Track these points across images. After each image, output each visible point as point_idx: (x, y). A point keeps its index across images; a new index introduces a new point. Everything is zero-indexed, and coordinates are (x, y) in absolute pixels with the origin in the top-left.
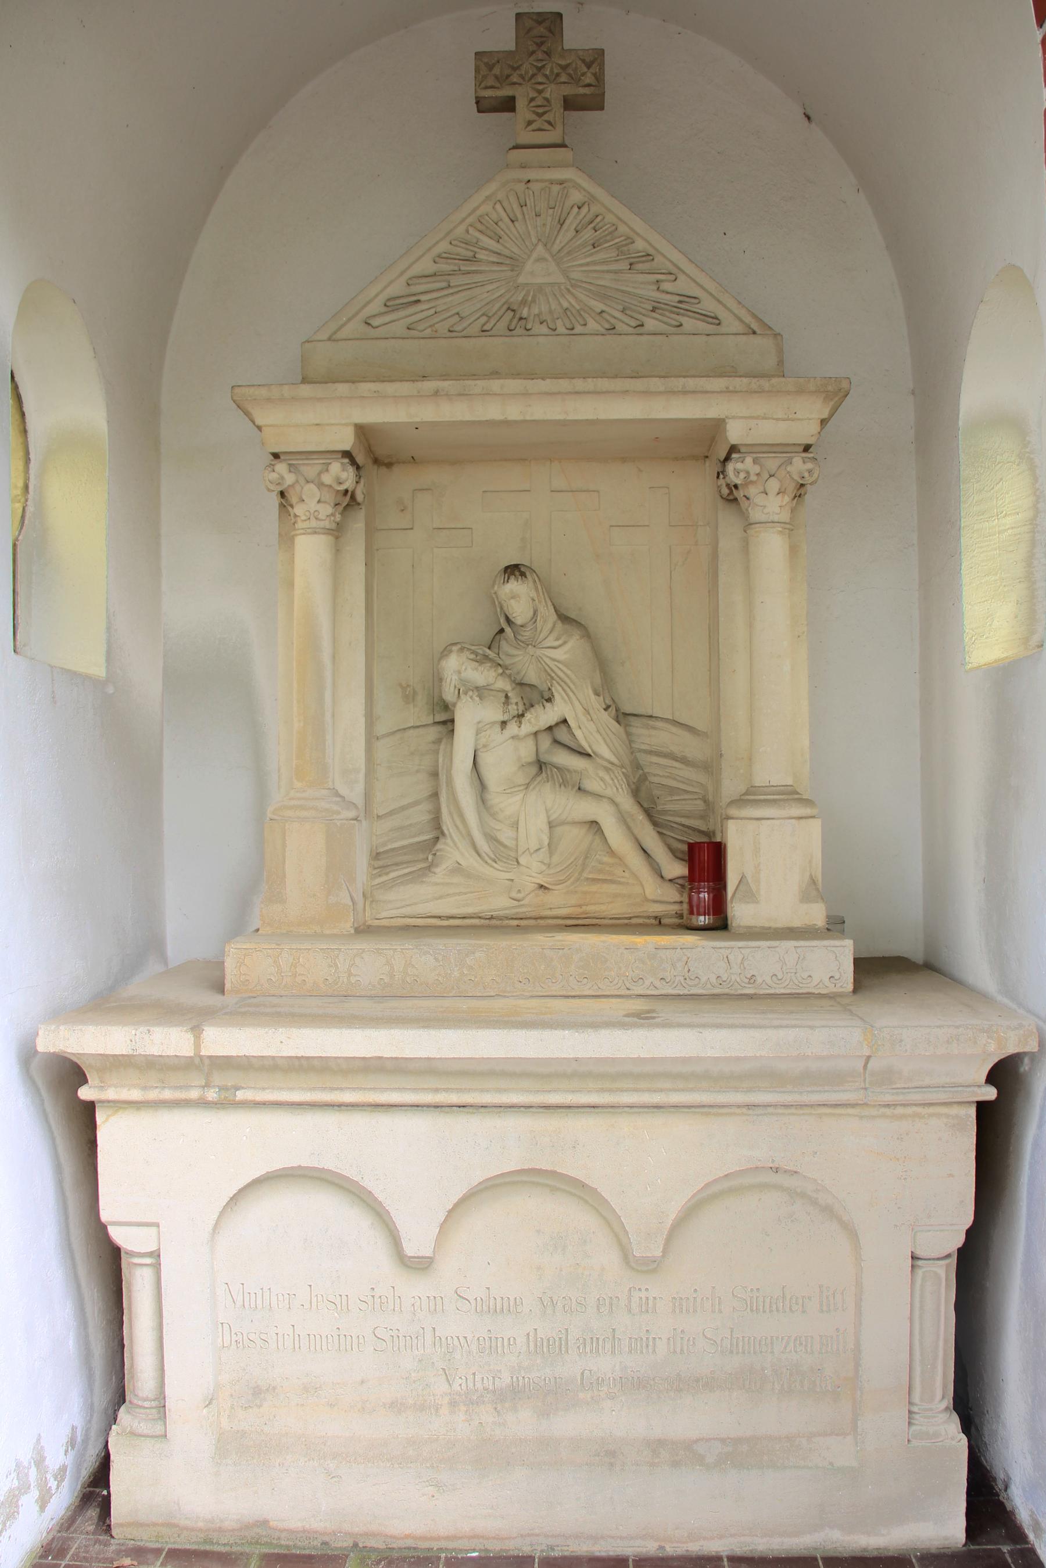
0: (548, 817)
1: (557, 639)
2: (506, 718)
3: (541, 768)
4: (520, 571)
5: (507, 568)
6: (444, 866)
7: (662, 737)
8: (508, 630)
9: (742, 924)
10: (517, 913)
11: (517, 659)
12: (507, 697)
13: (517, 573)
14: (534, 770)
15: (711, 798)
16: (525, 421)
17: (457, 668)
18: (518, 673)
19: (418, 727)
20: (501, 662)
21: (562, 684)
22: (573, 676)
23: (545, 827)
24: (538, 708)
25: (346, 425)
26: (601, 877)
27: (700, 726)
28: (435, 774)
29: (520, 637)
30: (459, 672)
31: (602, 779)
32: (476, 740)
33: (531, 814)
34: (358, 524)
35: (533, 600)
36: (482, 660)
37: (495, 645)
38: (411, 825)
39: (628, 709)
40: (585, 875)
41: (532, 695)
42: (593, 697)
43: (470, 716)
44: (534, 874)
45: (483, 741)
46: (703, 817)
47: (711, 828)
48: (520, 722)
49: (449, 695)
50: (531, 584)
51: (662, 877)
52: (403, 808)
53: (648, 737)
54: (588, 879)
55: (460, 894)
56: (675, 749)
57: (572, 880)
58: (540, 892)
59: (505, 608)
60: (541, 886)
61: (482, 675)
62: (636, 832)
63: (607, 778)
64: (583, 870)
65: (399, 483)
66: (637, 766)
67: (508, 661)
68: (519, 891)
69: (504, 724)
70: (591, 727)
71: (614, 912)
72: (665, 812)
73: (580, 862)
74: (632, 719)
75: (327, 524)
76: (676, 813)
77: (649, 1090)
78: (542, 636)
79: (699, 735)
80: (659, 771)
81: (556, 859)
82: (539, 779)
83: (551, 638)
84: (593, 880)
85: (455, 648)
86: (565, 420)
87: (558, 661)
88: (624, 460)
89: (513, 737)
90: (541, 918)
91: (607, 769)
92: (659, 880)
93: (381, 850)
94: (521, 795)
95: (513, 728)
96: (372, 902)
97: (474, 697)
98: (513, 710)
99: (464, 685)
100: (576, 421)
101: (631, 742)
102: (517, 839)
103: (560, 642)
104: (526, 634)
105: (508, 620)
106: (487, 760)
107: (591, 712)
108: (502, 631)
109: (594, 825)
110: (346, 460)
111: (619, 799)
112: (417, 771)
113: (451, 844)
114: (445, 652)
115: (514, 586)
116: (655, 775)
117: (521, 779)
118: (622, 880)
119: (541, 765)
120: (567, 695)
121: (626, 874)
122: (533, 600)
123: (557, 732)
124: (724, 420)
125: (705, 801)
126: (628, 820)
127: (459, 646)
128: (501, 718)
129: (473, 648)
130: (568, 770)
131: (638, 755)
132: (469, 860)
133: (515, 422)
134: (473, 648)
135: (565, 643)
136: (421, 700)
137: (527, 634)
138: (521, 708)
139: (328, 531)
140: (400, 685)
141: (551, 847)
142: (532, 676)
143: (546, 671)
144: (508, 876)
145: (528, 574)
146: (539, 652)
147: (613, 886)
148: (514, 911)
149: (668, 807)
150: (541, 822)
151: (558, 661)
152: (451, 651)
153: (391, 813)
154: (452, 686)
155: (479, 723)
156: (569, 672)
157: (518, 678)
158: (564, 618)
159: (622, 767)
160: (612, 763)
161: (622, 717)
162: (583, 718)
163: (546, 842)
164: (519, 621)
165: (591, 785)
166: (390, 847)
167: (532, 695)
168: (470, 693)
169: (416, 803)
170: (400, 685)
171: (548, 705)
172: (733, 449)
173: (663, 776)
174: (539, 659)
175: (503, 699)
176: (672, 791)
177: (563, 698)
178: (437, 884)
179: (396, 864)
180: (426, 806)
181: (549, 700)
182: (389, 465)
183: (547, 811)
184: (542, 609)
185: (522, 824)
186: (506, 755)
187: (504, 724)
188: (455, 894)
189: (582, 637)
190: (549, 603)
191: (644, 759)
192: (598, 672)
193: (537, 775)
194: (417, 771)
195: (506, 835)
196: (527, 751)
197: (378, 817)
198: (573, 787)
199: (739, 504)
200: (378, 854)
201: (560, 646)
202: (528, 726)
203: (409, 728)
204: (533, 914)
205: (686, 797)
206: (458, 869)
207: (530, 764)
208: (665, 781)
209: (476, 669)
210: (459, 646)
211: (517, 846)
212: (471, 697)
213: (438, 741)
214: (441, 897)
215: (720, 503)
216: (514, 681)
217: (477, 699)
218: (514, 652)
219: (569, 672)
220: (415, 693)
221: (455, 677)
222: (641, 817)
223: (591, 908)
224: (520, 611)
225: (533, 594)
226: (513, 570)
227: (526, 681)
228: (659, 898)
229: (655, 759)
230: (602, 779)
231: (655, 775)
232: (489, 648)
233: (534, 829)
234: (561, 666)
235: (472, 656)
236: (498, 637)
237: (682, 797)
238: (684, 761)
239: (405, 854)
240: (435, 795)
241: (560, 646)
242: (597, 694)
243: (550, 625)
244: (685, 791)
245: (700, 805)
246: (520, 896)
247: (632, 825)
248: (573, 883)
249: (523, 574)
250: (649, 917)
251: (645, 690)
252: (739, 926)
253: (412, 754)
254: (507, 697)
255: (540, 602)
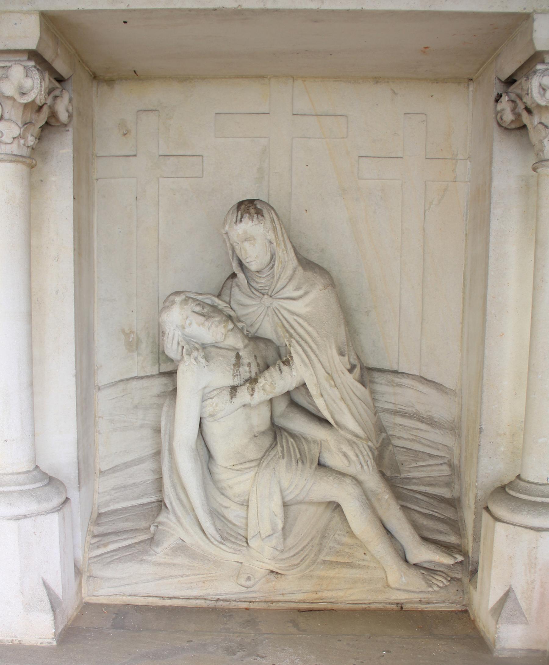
0: (283, 498)
1: (297, 289)
2: (236, 382)
3: (275, 438)
4: (255, 208)
5: (240, 204)
6: (166, 545)
7: (410, 396)
8: (241, 276)
9: (507, 646)
10: (246, 598)
11: (251, 310)
12: (238, 357)
13: (252, 211)
14: (267, 441)
15: (456, 462)
16: (266, 11)
17: (181, 323)
18: (252, 325)
19: (142, 378)
20: (232, 313)
21: (302, 343)
22: (315, 335)
23: (278, 509)
24: (273, 371)
25: (28, 12)
26: (340, 559)
27: (449, 383)
28: (157, 431)
29: (252, 284)
30: (184, 328)
31: (345, 455)
32: (202, 408)
33: (264, 493)
34: (63, 150)
35: (271, 243)
36: (210, 312)
37: (226, 291)
38: (134, 484)
39: (372, 362)
40: (322, 557)
41: (270, 354)
42: (337, 358)
43: (192, 378)
44: (266, 561)
45: (209, 410)
46: (448, 485)
47: (456, 494)
48: (253, 390)
49: (172, 351)
50: (269, 224)
51: (406, 561)
52: (127, 465)
53: (392, 395)
54: (325, 562)
55: (182, 576)
56: (421, 409)
57: (307, 562)
58: (272, 577)
59: (238, 252)
60: (272, 572)
61: (212, 332)
62: (381, 512)
63: (351, 454)
64: (319, 551)
65: (118, 106)
66: (380, 428)
67: (241, 312)
68: (249, 579)
69: (234, 389)
70: (335, 394)
71: (353, 598)
72: (409, 480)
73: (316, 541)
74: (376, 375)
75: (14, 148)
76: (420, 481)
77: (282, 232)
78: (280, 285)
79: (447, 393)
80: (404, 433)
81: (290, 541)
82: (273, 453)
83: (290, 287)
84: (332, 563)
85: (178, 299)
86: (319, 11)
87: (298, 315)
88: (377, 80)
89: (244, 406)
90: (273, 602)
91: (351, 443)
92: (404, 566)
93: (103, 510)
94: (253, 473)
95: (244, 395)
96: (89, 577)
97: (200, 359)
98: (245, 372)
99: (188, 343)
100: (333, 11)
101: (374, 400)
102: (247, 518)
103: (300, 292)
104: (262, 282)
105: (241, 264)
106: (214, 430)
107: (335, 376)
108: (234, 275)
109: (336, 507)
110: (32, 63)
111: (363, 477)
112: (142, 426)
113: (174, 520)
114: (166, 304)
115: (248, 226)
116: (399, 438)
117: (253, 453)
118: (365, 563)
119: (276, 431)
120: (308, 356)
121: (367, 557)
122: (271, 243)
123: (296, 401)
124: (531, 13)
125: (450, 465)
126: (373, 500)
127: (183, 297)
128: (230, 382)
129: (200, 297)
130: (306, 440)
131: (382, 415)
132: (193, 538)
133: (253, 11)
134: (200, 297)
135: (306, 293)
136: (145, 348)
137: (263, 281)
138: (254, 369)
139: (15, 158)
140: (123, 331)
141: (285, 531)
142: (267, 329)
143: (284, 326)
144: (237, 558)
145: (265, 212)
146: (276, 304)
147: (354, 571)
148: (245, 596)
149: (411, 475)
150: (276, 505)
151: (298, 315)
152: (173, 302)
153: (114, 469)
154: (175, 342)
155: (205, 388)
156: (310, 329)
157: (252, 330)
158: (306, 263)
159: (369, 439)
160: (357, 436)
161: (366, 374)
162: (325, 384)
163: (280, 525)
164: (253, 267)
165: (334, 459)
166: (112, 507)
167: (270, 354)
168: (195, 354)
169: (140, 461)
170: (123, 331)
171: (285, 368)
172: (537, 57)
173: (408, 439)
174: (276, 312)
175: (233, 360)
176: (417, 455)
177: (303, 361)
178: (158, 564)
179: (116, 533)
180: (149, 465)
181: (287, 363)
182: (110, 82)
183: (281, 491)
184: (280, 254)
185: (252, 504)
186: (235, 427)
187: (234, 389)
188: (179, 576)
189: (326, 286)
190: (289, 246)
191: (388, 420)
192: (343, 327)
193: (273, 446)
194: (142, 426)
195: (234, 513)
196: (260, 420)
197: (101, 472)
198: (311, 463)
199: (527, 135)
200: (100, 515)
201: (301, 297)
202: (260, 395)
203: (133, 378)
204: (264, 599)
205: (431, 462)
206: (181, 548)
207: (263, 433)
208: (409, 445)
209: (203, 324)
210: (183, 297)
211: (247, 525)
212: (196, 359)
213: (162, 395)
214: (162, 578)
215: (496, 133)
216: (247, 336)
217: (203, 361)
218: (248, 301)
219: (310, 329)
220: (139, 341)
221: (178, 333)
222: (387, 496)
223: (328, 595)
224: (255, 255)
225: (271, 236)
226: (248, 207)
227: (261, 333)
228: (403, 588)
229: (399, 420)
230: (345, 455)
231: (399, 438)
232: (219, 296)
233: (266, 512)
234: (301, 321)
235: (198, 309)
236: (229, 282)
237: (427, 463)
238: (431, 422)
239: (127, 520)
240: (158, 454)
241: (301, 297)
242: (342, 354)
243: (289, 272)
244: (430, 455)
245: (445, 470)
246: (249, 583)
247: (376, 505)
248: (308, 566)
249: (259, 212)
250: (392, 604)
251: (388, 345)
252: (504, 649)
253: (136, 407)
254: (238, 357)
255: (278, 245)
